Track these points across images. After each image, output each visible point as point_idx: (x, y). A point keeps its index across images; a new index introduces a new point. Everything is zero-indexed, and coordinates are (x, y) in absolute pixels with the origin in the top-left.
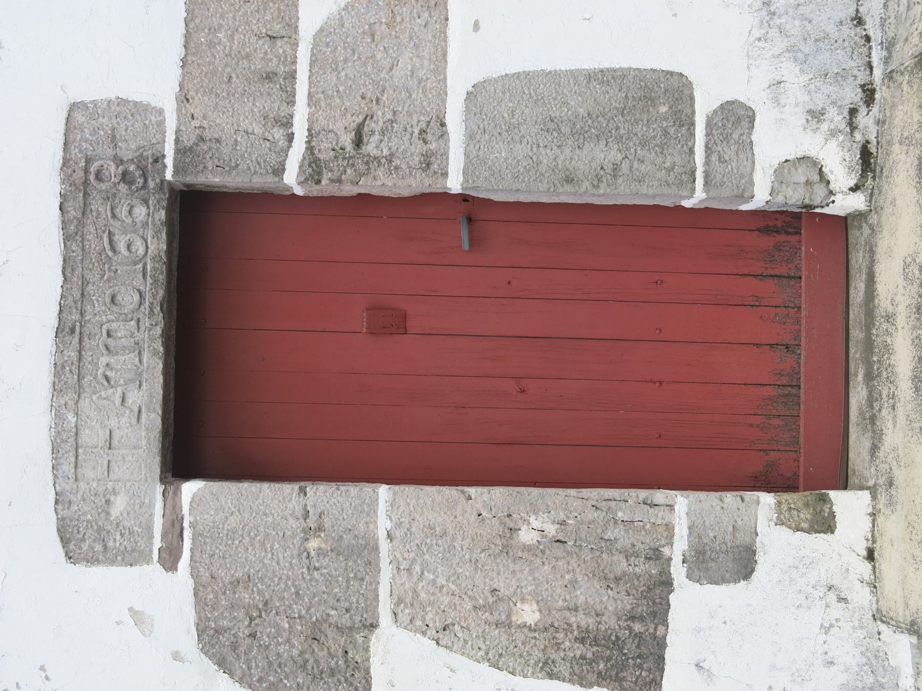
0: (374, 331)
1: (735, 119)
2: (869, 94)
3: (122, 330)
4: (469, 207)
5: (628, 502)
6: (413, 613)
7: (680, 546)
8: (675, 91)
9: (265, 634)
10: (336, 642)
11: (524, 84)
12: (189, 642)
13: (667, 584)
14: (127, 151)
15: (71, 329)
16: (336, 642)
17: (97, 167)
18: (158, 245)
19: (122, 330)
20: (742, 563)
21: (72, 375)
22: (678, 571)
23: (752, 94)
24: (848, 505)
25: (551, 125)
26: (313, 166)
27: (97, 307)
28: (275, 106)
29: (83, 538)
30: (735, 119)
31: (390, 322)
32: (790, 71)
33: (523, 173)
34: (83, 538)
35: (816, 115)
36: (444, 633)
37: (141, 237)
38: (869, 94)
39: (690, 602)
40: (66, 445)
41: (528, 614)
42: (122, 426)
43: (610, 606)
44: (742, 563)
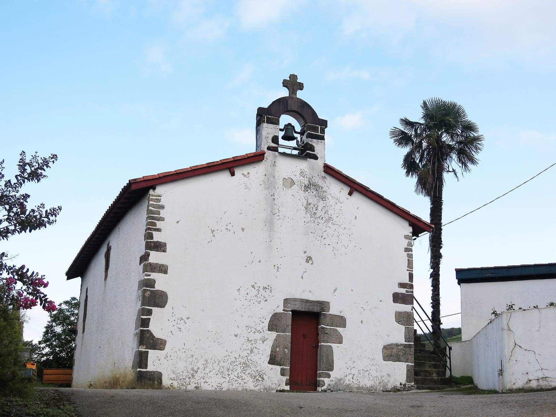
0: (304, 335)
1: (329, 376)
2: (332, 391)
3: (307, 307)
4: (317, 346)
5: (289, 361)
6: (278, 336)
7: (284, 367)
8: (332, 369)
9: (276, 320)
10: (275, 328)
11: (332, 352)
12: (275, 312)
13: (280, 366)
14: (325, 308)
15: (307, 301)
16: (275, 328)
17: (324, 305)
18: (315, 311)
19: (307, 307)
20: (282, 374)
21: (302, 301)
22: (282, 367)
23: (332, 378)
24: (288, 388)
25: (328, 355)
26: (323, 328)
27: (309, 304)
28: (329, 324)
29: (286, 301)
30: (329, 376)
31: (304, 336)
32: (334, 382)
33: (322, 353)
34: (286, 301)
35: (329, 385)
36: (276, 340)
37: (316, 309)
38: (332, 391)
39: (279, 368)
40: (295, 300)
41: (278, 350)
42: (297, 306)
43: (278, 359)
44: (282, 374)
